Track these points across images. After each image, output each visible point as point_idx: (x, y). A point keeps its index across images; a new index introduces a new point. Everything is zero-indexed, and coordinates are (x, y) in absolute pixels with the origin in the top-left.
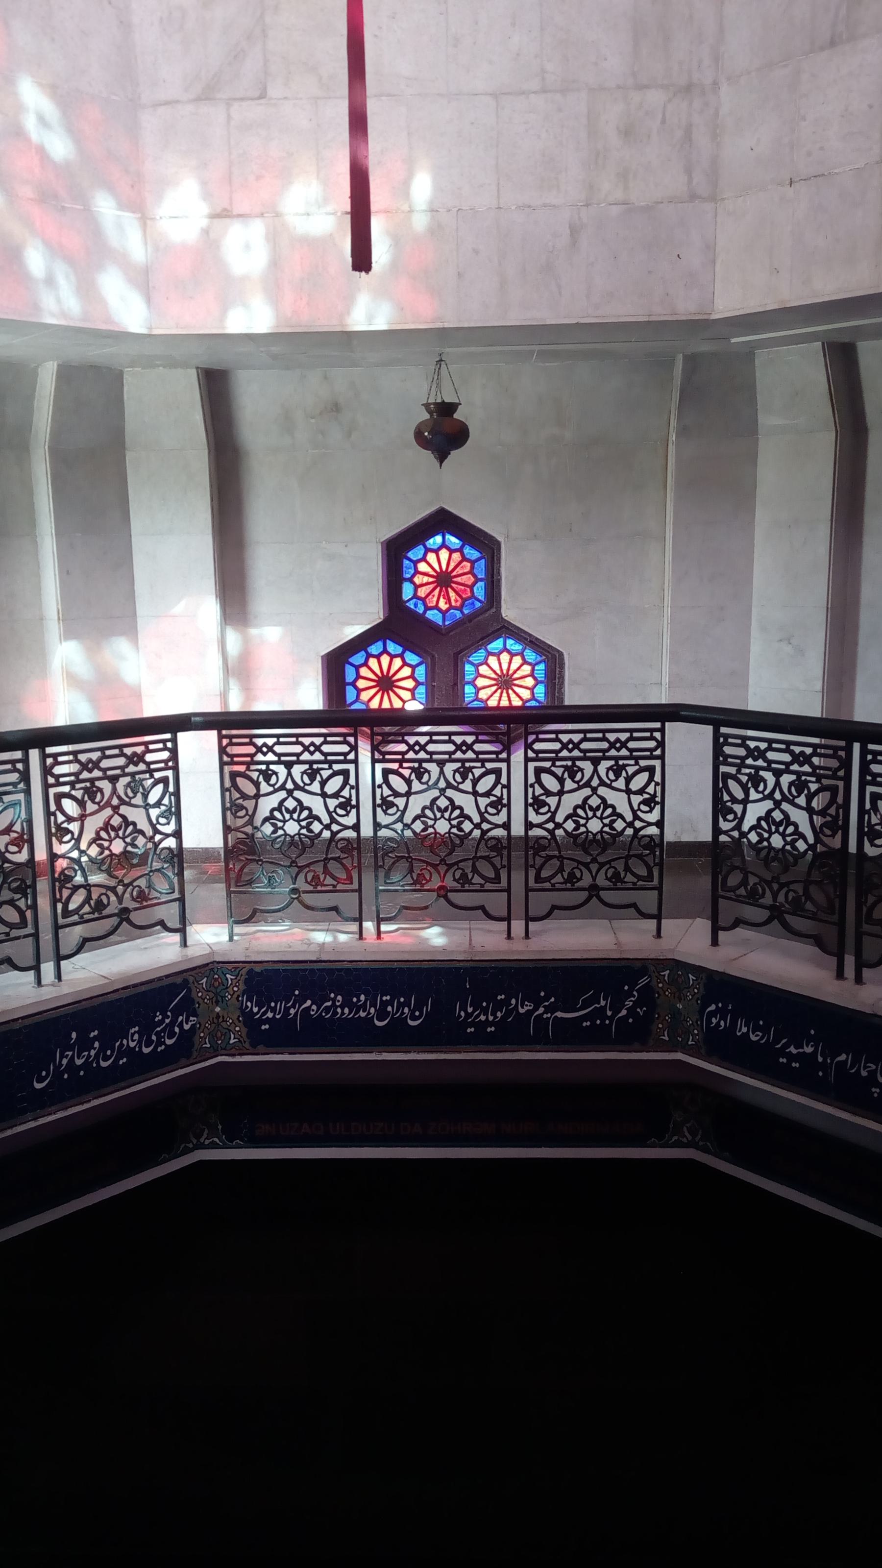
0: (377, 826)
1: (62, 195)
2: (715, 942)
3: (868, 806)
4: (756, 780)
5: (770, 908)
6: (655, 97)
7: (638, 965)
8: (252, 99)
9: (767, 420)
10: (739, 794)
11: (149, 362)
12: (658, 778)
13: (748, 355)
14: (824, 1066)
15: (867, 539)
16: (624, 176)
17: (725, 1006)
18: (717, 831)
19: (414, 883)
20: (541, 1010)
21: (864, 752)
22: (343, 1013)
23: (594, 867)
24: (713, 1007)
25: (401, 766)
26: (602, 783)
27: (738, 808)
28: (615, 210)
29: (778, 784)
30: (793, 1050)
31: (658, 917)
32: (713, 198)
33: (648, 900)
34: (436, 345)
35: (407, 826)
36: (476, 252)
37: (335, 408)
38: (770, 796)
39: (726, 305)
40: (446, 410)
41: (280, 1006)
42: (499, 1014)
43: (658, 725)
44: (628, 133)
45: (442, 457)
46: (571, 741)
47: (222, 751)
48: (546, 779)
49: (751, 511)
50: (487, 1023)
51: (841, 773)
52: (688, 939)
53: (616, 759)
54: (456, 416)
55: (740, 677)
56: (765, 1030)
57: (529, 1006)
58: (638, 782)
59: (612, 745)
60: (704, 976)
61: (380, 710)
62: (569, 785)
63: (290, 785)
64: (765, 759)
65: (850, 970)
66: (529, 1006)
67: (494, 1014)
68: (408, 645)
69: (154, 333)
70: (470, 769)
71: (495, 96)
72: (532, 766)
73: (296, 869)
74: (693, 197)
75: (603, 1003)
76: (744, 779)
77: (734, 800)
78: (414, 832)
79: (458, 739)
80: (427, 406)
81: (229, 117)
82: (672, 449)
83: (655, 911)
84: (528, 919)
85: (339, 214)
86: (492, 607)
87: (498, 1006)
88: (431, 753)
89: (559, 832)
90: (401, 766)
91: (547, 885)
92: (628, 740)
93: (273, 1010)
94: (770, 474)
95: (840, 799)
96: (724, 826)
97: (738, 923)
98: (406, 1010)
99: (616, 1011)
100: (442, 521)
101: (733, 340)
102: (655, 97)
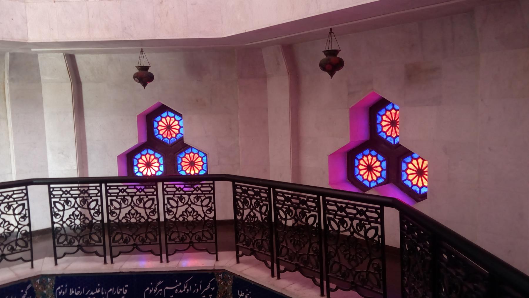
2: (56, 264)
3: (109, 204)
4: (67, 202)
5: (78, 246)
7: (26, 281)
9: (43, 77)
10: (61, 208)
12: (156, 202)
13: (35, 55)
14: (105, 295)
17: (64, 286)
18: (53, 223)
21: (106, 186)
24: (59, 288)
29: (132, 200)
30: (92, 293)
31: (32, 260)
33: (26, 255)
39: (33, 37)
47: (50, 193)
49: (42, 108)
51: (99, 194)
52: (45, 266)
55: (45, 167)
56: (81, 290)
58: (205, 203)
60: (54, 277)
64: (70, 194)
65: (164, 259)
82: (7, 87)
83: (30, 258)
96: (55, 220)
97: (176, 251)
101: (32, 50)
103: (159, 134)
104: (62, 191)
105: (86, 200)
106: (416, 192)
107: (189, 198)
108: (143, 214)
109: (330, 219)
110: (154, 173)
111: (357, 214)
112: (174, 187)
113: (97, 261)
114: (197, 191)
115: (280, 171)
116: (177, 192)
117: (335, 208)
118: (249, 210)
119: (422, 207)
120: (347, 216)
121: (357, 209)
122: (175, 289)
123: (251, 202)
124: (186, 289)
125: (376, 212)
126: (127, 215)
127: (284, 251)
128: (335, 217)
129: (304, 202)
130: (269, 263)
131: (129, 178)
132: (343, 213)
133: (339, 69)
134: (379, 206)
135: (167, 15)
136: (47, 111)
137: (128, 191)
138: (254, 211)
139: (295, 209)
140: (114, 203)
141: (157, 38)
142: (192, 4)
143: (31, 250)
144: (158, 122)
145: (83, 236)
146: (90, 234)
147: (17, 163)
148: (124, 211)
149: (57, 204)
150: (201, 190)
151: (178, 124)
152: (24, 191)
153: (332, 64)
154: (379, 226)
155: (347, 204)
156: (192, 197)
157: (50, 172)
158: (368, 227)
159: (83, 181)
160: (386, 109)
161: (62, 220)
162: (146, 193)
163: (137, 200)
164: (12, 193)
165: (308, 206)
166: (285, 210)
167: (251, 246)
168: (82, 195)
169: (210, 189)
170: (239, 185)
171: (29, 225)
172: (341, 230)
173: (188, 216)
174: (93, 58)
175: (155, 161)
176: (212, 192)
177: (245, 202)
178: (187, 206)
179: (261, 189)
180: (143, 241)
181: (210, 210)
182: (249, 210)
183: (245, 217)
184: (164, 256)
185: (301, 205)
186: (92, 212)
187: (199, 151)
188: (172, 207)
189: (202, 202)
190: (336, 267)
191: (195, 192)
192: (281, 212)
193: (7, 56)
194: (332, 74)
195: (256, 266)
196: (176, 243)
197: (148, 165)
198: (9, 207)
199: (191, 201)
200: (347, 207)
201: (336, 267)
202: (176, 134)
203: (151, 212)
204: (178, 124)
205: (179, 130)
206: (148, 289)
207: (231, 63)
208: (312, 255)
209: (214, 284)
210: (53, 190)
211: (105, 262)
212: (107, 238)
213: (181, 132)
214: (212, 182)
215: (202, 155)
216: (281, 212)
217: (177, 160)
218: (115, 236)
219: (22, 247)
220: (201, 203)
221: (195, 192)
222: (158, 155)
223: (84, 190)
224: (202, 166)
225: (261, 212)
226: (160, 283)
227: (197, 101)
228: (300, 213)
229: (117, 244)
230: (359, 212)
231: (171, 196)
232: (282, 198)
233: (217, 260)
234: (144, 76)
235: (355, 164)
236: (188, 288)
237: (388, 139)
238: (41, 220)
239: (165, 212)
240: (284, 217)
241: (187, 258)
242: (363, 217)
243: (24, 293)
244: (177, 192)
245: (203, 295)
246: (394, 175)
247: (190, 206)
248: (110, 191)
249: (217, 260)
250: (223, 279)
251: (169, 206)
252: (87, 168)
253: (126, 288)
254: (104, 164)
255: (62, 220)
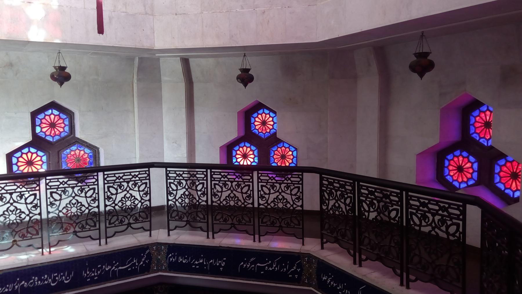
0: (48, 213)
2: (169, 235)
3: (213, 187)
5: (187, 221)
7: (146, 247)
9: (164, 78)
10: (175, 188)
13: (158, 59)
14: (206, 265)
15: (195, 113)
17: (174, 254)
18: (168, 200)
19: (64, 231)
20: (114, 268)
21: (211, 172)
22: (38, 283)
23: (129, 217)
25: (57, 190)
26: (130, 189)
27: (175, 192)
29: (232, 185)
30: (196, 263)
31: (150, 230)
32: (152, 15)
33: (146, 225)
34: (58, 49)
35: (60, 211)
38: (185, 187)
39: (159, 45)
41: (11, 286)
42: (99, 272)
43: (147, 169)
46: (119, 176)
47: (167, 175)
48: (112, 190)
50: (95, 276)
51: (205, 179)
52: (160, 236)
53: (135, 181)
55: (162, 154)
56: (188, 259)
57: (109, 267)
59: (133, 177)
60: (167, 246)
61: (28, 173)
62: (119, 191)
63: (11, 201)
64: (182, 177)
66: (109, 267)
67: (97, 272)
68: (39, 149)
70: (137, 183)
72: (49, 191)
73: (15, 233)
74: (146, 14)
75: (135, 261)
76: (176, 183)
77: (173, 190)
78: (63, 213)
79: (61, 180)
80: (55, 67)
83: (149, 228)
84: (107, 238)
86: (72, 134)
87: (98, 269)
88: (69, 185)
89: (117, 207)
90: (57, 190)
91: (113, 225)
92: (123, 176)
93: (8, 288)
94: (166, 93)
95: (205, 186)
96: (170, 198)
97: (267, 233)
98: (64, 277)
99: (139, 263)
100: (53, 105)
103: (255, 129)
104: (176, 174)
105: (195, 183)
106: (510, 196)
107: (280, 187)
108: (241, 198)
109: (412, 213)
110: (249, 163)
111: (439, 210)
112: (268, 176)
113: (201, 236)
114: (287, 181)
115: (366, 166)
116: (270, 181)
117: (417, 203)
118: (334, 201)
119: (515, 212)
120: (429, 212)
121: (439, 206)
122: (265, 266)
123: (336, 194)
124: (275, 268)
125: (458, 209)
126: (227, 198)
127: (366, 241)
128: (417, 212)
129: (387, 197)
130: (352, 252)
131: (228, 165)
132: (426, 209)
133: (429, 70)
134: (461, 204)
135: (268, 24)
136: (165, 107)
137: (229, 177)
138: (339, 202)
139: (379, 202)
140: (217, 186)
141: (258, 44)
142: (290, 13)
143: (150, 221)
144: (255, 118)
145: (191, 213)
146: (197, 212)
147: (141, 149)
148: (225, 194)
149: (172, 185)
150: (291, 180)
151: (273, 121)
152: (147, 172)
153: (422, 65)
154: (461, 223)
155: (429, 200)
156: (283, 186)
157: (165, 158)
158: (449, 223)
159: (191, 166)
160: (480, 110)
161: (175, 198)
162: (243, 179)
163: (236, 185)
164: (138, 173)
165: (391, 201)
166: (368, 202)
167: (335, 235)
168: (192, 178)
169: (298, 179)
170: (325, 178)
171: (150, 200)
172: (423, 224)
173: (278, 203)
174: (203, 62)
175: (251, 153)
176: (301, 182)
177: (330, 194)
178: (278, 194)
179: (346, 182)
180: (240, 221)
181: (298, 198)
182: (334, 201)
183: (330, 207)
184: (257, 236)
185: (384, 199)
186: (199, 193)
187: (290, 145)
188: (265, 194)
189: (291, 191)
190: (416, 259)
191: (286, 181)
192: (364, 204)
193: (137, 61)
194: (421, 75)
195: (339, 253)
196: (267, 226)
197: (245, 156)
198: (21, 197)
199: (282, 189)
200: (429, 203)
201: (416, 259)
202: (270, 130)
203: (247, 196)
204: (273, 121)
205: (273, 125)
206: (242, 263)
207: (325, 66)
208: (393, 247)
209: (300, 266)
210: (170, 173)
211: (208, 237)
212: (210, 217)
213: (275, 128)
214: (301, 173)
215: (293, 149)
216: (364, 204)
217: (269, 153)
218: (217, 215)
219: (143, 218)
220: (291, 192)
221: (286, 181)
222: (253, 148)
223: (179, 174)
224: (292, 159)
225: (345, 203)
226: (252, 259)
227: (290, 99)
228: (383, 206)
229: (218, 222)
230: (441, 208)
231: (265, 184)
232: (366, 192)
233: (303, 245)
234: (245, 78)
235: (445, 164)
236: (277, 266)
237: (481, 141)
238: (159, 198)
239: (258, 197)
240: (367, 209)
241: (276, 240)
242: (445, 213)
243: (143, 256)
244: (270, 181)
245: (290, 274)
246: (486, 177)
247: (280, 193)
248: (214, 176)
249: (303, 245)
250: (308, 262)
251: (262, 193)
252: (195, 156)
253: (224, 261)
254: (209, 154)
255: (175, 198)
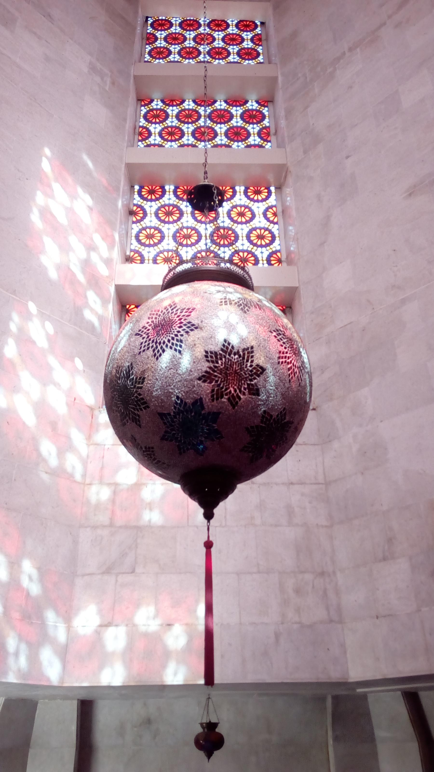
1: (31, 615)
6: (308, 577)
8: (128, 573)
9: (380, 733)
11: (53, 698)
13: (364, 697)
16: (298, 610)
28: (295, 626)
32: (341, 622)
36: (230, 645)
37: (148, 721)
39: (356, 674)
40: (211, 726)
44: (298, 591)
45: (209, 755)
54: (217, 730)
69: (63, 686)
71: (238, 574)
74: (331, 621)
80: (202, 724)
81: (117, 581)
85: (164, 625)
102: (308, 577)
